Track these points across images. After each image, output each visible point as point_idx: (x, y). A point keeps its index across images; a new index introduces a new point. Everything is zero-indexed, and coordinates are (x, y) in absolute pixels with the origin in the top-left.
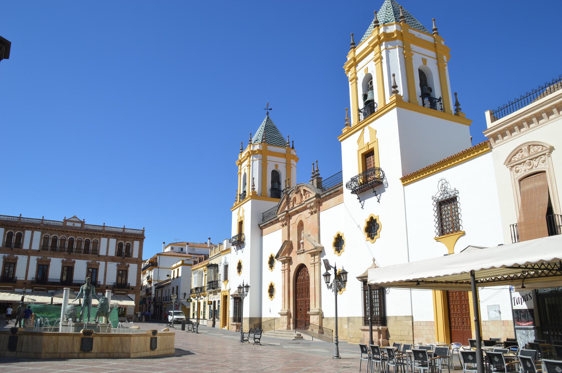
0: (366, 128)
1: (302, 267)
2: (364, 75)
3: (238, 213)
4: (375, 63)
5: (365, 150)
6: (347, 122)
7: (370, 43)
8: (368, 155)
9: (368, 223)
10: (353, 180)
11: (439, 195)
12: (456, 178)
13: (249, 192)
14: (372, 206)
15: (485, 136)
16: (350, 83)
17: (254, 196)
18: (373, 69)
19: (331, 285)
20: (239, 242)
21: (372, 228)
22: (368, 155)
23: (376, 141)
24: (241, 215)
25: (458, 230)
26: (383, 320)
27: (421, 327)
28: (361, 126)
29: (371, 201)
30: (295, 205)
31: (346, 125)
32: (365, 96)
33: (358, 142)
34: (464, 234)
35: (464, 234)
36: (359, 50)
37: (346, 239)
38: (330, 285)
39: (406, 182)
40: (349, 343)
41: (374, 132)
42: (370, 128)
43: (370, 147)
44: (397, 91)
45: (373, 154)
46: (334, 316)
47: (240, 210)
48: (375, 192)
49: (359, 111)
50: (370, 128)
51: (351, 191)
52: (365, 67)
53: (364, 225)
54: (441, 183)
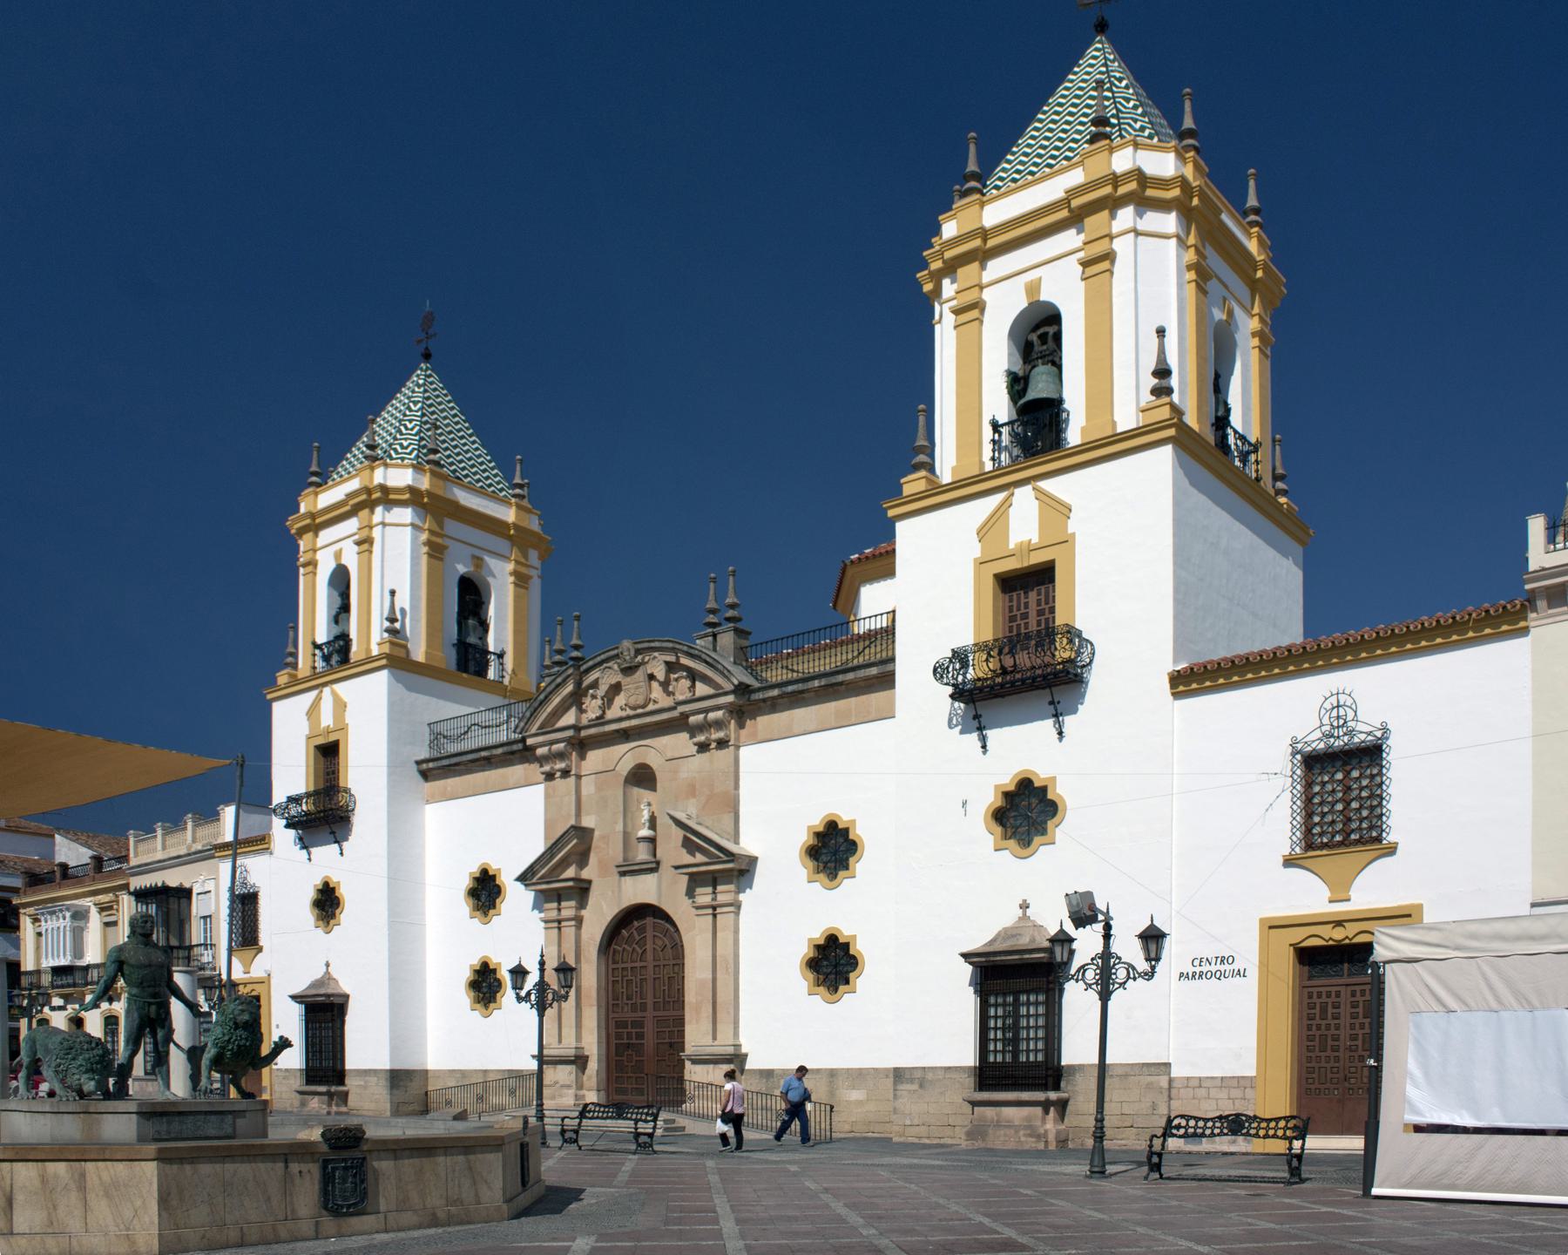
0: (327, 690)
1: (636, 920)
2: (1023, 304)
3: (313, 711)
4: (356, 548)
5: (321, 741)
6: (290, 659)
7: (350, 496)
8: (328, 753)
9: (320, 891)
10: (291, 799)
11: (1318, 734)
12: (1381, 694)
13: (369, 637)
14: (326, 861)
15: (1527, 587)
16: (302, 570)
17: (398, 661)
18: (1065, 289)
19: (529, 994)
20: (325, 817)
21: (327, 902)
22: (328, 753)
23: (343, 729)
24: (327, 720)
25: (1378, 840)
26: (339, 1076)
27: (1202, 1092)
28: (316, 681)
29: (326, 854)
30: (610, 715)
31: (287, 665)
32: (1017, 384)
33: (983, 532)
34: (1392, 850)
35: (1392, 850)
36: (995, 213)
37: (308, 915)
38: (523, 993)
39: (1181, 688)
40: (896, 1139)
41: (340, 706)
42: (334, 693)
43: (332, 738)
44: (1169, 391)
45: (1052, 580)
46: (1096, 1061)
47: (318, 699)
48: (333, 833)
49: (316, 646)
50: (334, 693)
51: (950, 690)
52: (336, 547)
53: (310, 894)
54: (1334, 700)
